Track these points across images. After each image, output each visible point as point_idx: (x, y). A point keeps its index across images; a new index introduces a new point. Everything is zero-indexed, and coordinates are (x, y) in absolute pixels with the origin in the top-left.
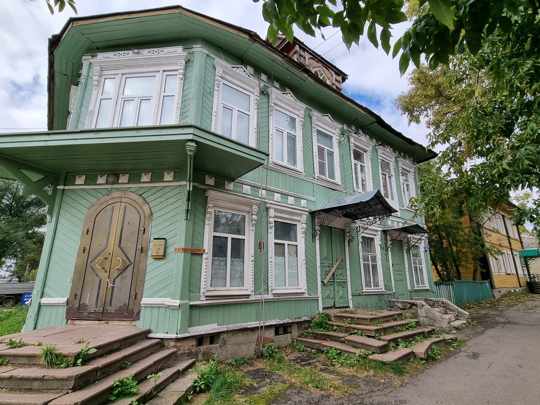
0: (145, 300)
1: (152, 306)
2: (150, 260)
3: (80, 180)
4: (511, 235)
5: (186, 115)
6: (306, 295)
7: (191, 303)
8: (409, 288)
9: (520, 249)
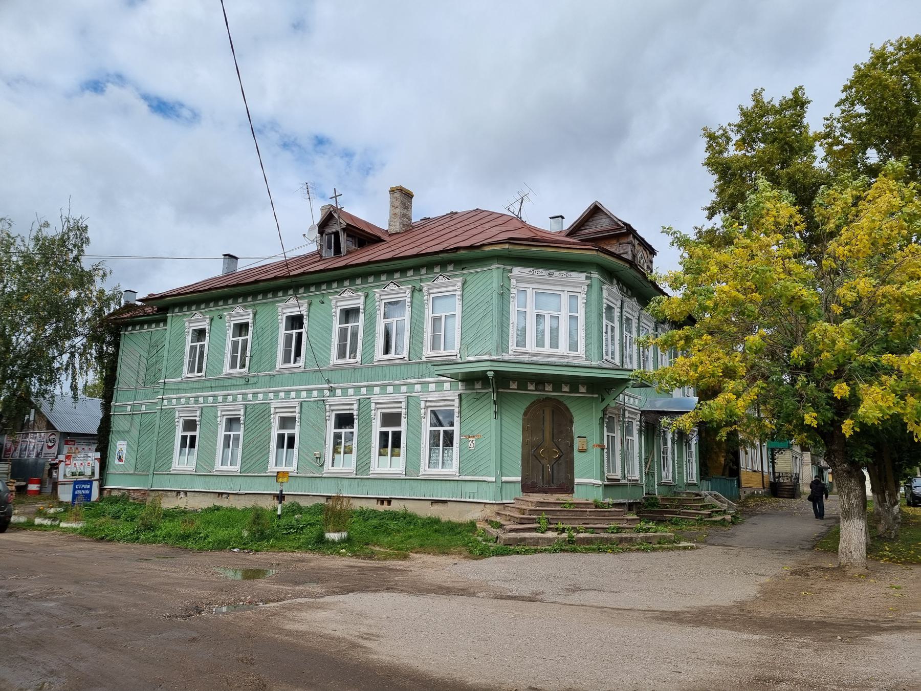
0: (576, 480)
2: (576, 453)
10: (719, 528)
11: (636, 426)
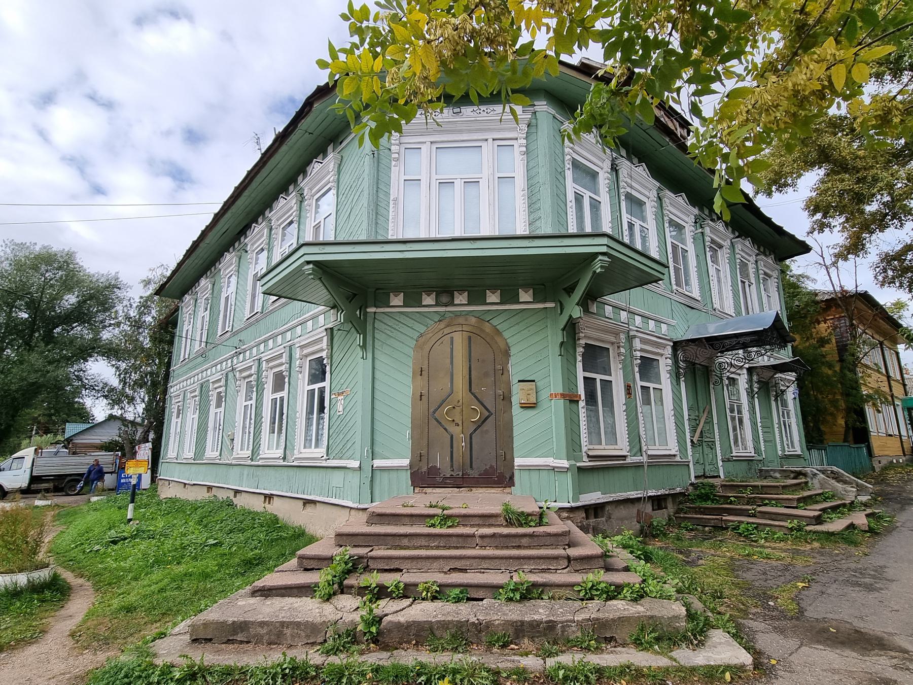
0: (518, 461)
1: (529, 469)
2: (516, 410)
3: (397, 300)
4: (892, 374)
5: (537, 206)
6: (678, 459)
7: (578, 464)
8: (780, 453)
9: (902, 396)
10: (840, 549)
11: (665, 366)
